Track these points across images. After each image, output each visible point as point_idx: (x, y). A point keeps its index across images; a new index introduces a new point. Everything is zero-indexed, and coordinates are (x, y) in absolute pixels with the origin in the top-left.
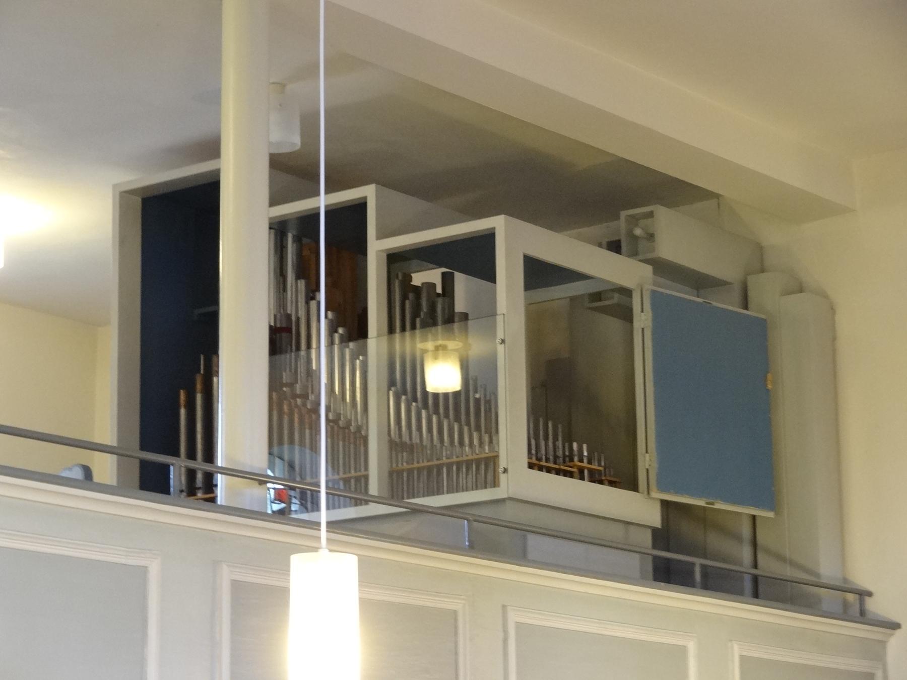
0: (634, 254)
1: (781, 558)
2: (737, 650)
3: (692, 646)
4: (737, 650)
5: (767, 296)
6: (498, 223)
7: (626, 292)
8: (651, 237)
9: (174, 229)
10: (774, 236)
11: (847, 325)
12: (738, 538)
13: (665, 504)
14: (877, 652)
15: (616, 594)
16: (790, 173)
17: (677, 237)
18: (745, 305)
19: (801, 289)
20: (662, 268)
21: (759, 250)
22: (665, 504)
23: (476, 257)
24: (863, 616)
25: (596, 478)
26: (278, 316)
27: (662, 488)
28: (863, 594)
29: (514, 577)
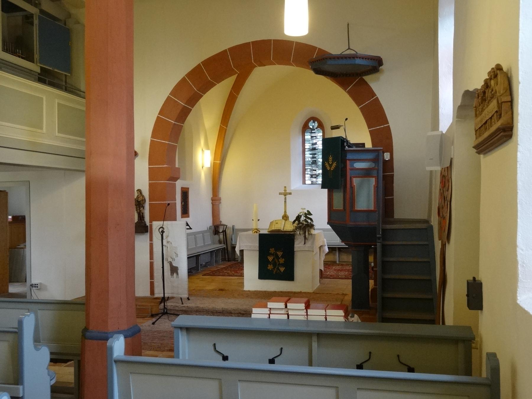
2: (57, 101)
3: (44, 98)
4: (57, 101)
7: (33, 14)
10: (73, 11)
12: (62, 80)
20: (42, 12)
22: (42, 68)
26: (204, 273)
27: (40, 63)
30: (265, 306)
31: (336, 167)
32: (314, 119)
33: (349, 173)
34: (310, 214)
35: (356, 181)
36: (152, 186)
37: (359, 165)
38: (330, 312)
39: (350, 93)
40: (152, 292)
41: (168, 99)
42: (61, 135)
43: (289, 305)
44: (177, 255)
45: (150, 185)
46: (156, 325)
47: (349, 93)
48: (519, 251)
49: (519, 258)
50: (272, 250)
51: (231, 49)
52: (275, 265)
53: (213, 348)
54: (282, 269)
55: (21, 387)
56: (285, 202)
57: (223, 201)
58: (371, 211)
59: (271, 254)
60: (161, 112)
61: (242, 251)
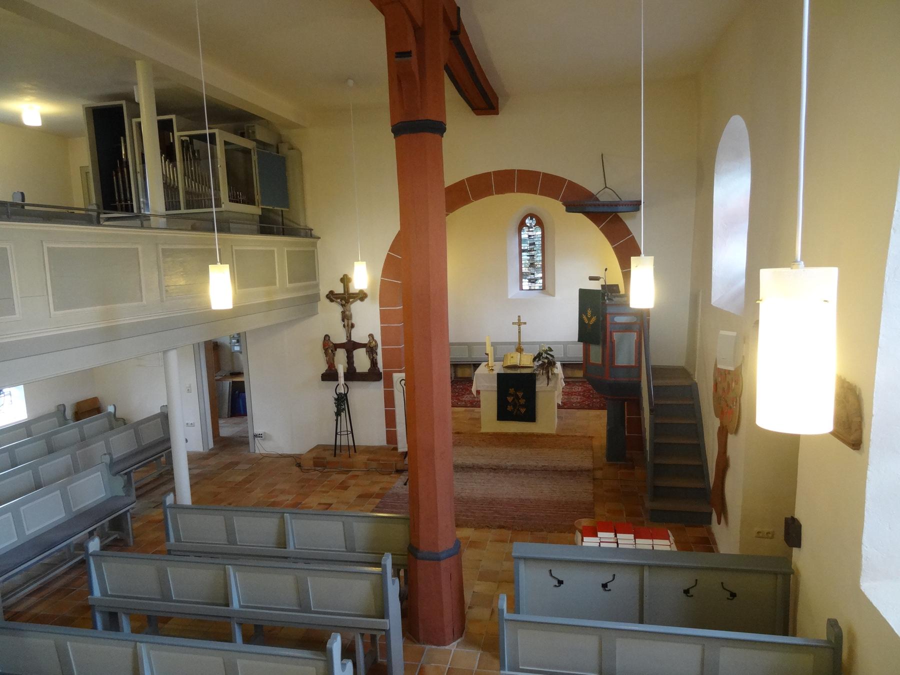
0: (249, 138)
1: (290, 220)
3: (276, 249)
5: (284, 149)
8: (254, 132)
9: (108, 124)
10: (284, 132)
11: (305, 158)
13: (262, 209)
14: (314, 245)
16: (292, 118)
17: (261, 134)
18: (278, 152)
21: (280, 136)
22: (262, 209)
24: (311, 236)
25: (244, 203)
28: (311, 230)
30: (597, 536)
32: (532, 216)
33: (609, 328)
34: (551, 350)
35: (616, 336)
38: (656, 541)
40: (391, 437)
42: (292, 285)
45: (382, 329)
47: (601, 229)
48: (864, 548)
49: (863, 553)
50: (512, 391)
51: (469, 179)
53: (548, 574)
54: (523, 410)
58: (632, 367)
59: (511, 395)
60: (392, 249)
61: (478, 392)
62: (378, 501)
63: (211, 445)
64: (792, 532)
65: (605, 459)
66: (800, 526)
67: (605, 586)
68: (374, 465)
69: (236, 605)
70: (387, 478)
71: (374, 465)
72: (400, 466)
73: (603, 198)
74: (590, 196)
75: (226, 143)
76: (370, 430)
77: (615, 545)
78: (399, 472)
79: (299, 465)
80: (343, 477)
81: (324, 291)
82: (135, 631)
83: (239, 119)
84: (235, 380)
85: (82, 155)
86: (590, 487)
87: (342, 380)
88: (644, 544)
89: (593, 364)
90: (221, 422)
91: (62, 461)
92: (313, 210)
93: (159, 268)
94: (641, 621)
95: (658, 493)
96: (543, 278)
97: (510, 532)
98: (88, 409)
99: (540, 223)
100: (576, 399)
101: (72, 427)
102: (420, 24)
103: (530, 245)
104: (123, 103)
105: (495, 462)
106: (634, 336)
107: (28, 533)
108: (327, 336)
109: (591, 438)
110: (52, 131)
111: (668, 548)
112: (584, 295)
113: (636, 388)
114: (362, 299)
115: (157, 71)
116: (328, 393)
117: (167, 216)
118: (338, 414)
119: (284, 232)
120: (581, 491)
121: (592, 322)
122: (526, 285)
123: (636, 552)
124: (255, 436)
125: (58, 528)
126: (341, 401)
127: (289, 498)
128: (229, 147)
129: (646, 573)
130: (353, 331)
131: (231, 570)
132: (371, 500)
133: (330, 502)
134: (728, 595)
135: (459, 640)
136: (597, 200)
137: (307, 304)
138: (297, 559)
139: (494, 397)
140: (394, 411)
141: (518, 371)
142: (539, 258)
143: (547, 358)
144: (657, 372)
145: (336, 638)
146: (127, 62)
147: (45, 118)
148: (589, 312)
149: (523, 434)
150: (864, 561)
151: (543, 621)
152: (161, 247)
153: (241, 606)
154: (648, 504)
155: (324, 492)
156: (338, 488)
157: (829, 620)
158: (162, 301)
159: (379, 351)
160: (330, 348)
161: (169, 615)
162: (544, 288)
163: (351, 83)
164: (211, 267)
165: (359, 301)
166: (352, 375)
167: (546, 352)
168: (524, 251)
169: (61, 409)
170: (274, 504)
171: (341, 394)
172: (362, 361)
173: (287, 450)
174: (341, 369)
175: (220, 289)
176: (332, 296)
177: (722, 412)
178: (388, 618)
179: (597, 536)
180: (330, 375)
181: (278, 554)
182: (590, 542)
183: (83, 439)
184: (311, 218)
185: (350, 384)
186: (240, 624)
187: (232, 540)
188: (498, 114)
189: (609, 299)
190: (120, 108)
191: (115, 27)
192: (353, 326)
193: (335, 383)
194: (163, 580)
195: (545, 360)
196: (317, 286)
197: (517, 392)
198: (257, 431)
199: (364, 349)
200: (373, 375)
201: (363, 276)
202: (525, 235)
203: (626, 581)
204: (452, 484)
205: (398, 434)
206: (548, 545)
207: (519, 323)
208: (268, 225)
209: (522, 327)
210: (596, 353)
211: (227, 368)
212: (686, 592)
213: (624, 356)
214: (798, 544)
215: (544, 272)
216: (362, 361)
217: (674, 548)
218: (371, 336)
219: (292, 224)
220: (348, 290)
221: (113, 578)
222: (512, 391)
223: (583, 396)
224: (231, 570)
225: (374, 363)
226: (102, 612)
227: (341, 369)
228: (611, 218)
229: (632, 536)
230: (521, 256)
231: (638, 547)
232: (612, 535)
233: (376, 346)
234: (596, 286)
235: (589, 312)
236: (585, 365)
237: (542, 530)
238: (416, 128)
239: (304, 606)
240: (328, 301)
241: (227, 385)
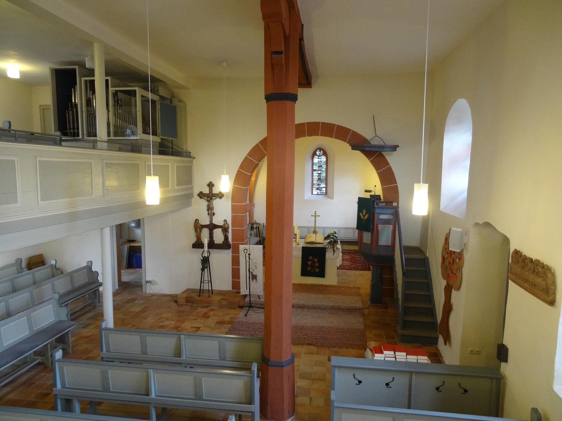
2: (176, 164)
5: (175, 102)
6: (137, 89)
8: (158, 90)
9: (65, 80)
10: (175, 91)
14: (192, 162)
15: (5, 146)
17: (162, 92)
19: (181, 102)
23: (132, 94)
24: (190, 157)
28: (190, 153)
29: (5, 146)
30: (382, 353)
31: (368, 218)
32: (320, 149)
34: (336, 233)
35: (380, 227)
36: (233, 218)
37: (382, 217)
38: (420, 357)
39: (372, 162)
41: (246, 158)
43: (396, 353)
44: (256, 267)
45: (233, 216)
46: (248, 316)
47: (371, 161)
52: (312, 267)
54: (317, 270)
55: (253, 406)
56: (315, 221)
57: (256, 206)
59: (310, 260)
60: (241, 167)
62: (230, 326)
63: (117, 287)
64: (502, 353)
65: (369, 302)
66: (507, 350)
67: (387, 384)
68: (224, 302)
69: (153, 395)
70: (233, 311)
71: (224, 302)
72: (241, 304)
73: (373, 143)
74: (365, 141)
75: (142, 96)
76: (222, 281)
77: (394, 359)
78: (241, 307)
79: (176, 302)
80: (205, 310)
81: (196, 191)
82: (83, 411)
83: (150, 82)
84: (132, 245)
85: (46, 97)
86: (361, 320)
87: (206, 248)
88: (412, 358)
89: (366, 244)
90: (122, 271)
91: (22, 297)
92: (191, 139)
93: (103, 175)
94: (409, 407)
95: (406, 325)
96: (326, 188)
97: (315, 347)
98: (36, 262)
99: (325, 154)
100: (347, 263)
101: (28, 274)
102: (288, 35)
103: (319, 167)
104: (77, 67)
105: (301, 302)
106: (391, 227)
107: (5, 345)
108: (197, 220)
109: (359, 288)
110: (27, 83)
111: (426, 362)
112: (361, 202)
113: (391, 259)
114: (221, 198)
115: (107, 50)
116: (197, 256)
117: (109, 141)
118: (203, 270)
119: (172, 154)
120: (355, 322)
121: (366, 218)
122: (315, 192)
123: (407, 363)
124: (147, 282)
125: (25, 341)
126: (205, 262)
127: (172, 323)
128: (144, 99)
129: (414, 377)
130: (214, 217)
131: (151, 372)
132: (225, 325)
133: (199, 326)
134: (463, 391)
135: (292, 418)
136: (370, 143)
137: (185, 199)
138: (192, 365)
139: (300, 261)
140: (239, 268)
141: (314, 246)
142: (324, 175)
143: (333, 238)
144: (407, 249)
145: (232, 419)
146: (87, 43)
147: (22, 74)
148: (364, 211)
149: (316, 285)
150: (556, 374)
151: (383, 410)
152: (105, 161)
153: (156, 396)
154: (400, 332)
155: (193, 319)
156: (202, 317)
157: (532, 408)
158: (104, 196)
159: (230, 230)
160: (198, 227)
161: (100, 401)
162: (326, 194)
163: (225, 64)
164: (147, 177)
165: (218, 199)
166: (212, 245)
167: (332, 234)
168: (315, 170)
169: (19, 261)
170: (162, 327)
171: (205, 257)
172: (219, 236)
173: (167, 292)
174: (206, 241)
175: (152, 192)
176: (201, 195)
177: (448, 276)
178: (254, 404)
179: (382, 353)
180: (198, 245)
181: (176, 362)
182: (378, 357)
183: (35, 283)
184: (190, 146)
185: (211, 250)
186: (155, 407)
187: (144, 352)
188: (311, 87)
189: (377, 204)
190: (74, 70)
191: (82, 20)
192: (214, 214)
193: (202, 250)
194: (105, 378)
195: (332, 239)
196: (192, 188)
197: (313, 259)
198: (148, 279)
199: (221, 229)
200: (225, 245)
201: (225, 184)
202: (316, 160)
203: (401, 381)
204: (289, 319)
205: (241, 283)
206: (339, 357)
207: (315, 216)
208: (164, 149)
209: (317, 218)
210: (367, 237)
211: (126, 237)
212: (437, 389)
213: (385, 239)
214: (506, 361)
215: (326, 184)
216: (219, 236)
217: (430, 362)
218: (225, 221)
219: (178, 149)
220: (212, 192)
221: (70, 375)
222: (311, 258)
223: (351, 261)
224: (151, 372)
225: (226, 238)
226: (62, 399)
227: (206, 241)
228: (376, 153)
229: (404, 354)
230: (313, 174)
231: (409, 360)
232: (392, 353)
233: (228, 227)
234: (367, 196)
235: (364, 211)
236: (359, 242)
237: (335, 347)
238: (279, 98)
239: (198, 396)
240: (198, 198)
241: (126, 248)
